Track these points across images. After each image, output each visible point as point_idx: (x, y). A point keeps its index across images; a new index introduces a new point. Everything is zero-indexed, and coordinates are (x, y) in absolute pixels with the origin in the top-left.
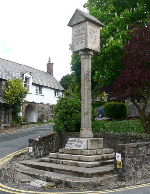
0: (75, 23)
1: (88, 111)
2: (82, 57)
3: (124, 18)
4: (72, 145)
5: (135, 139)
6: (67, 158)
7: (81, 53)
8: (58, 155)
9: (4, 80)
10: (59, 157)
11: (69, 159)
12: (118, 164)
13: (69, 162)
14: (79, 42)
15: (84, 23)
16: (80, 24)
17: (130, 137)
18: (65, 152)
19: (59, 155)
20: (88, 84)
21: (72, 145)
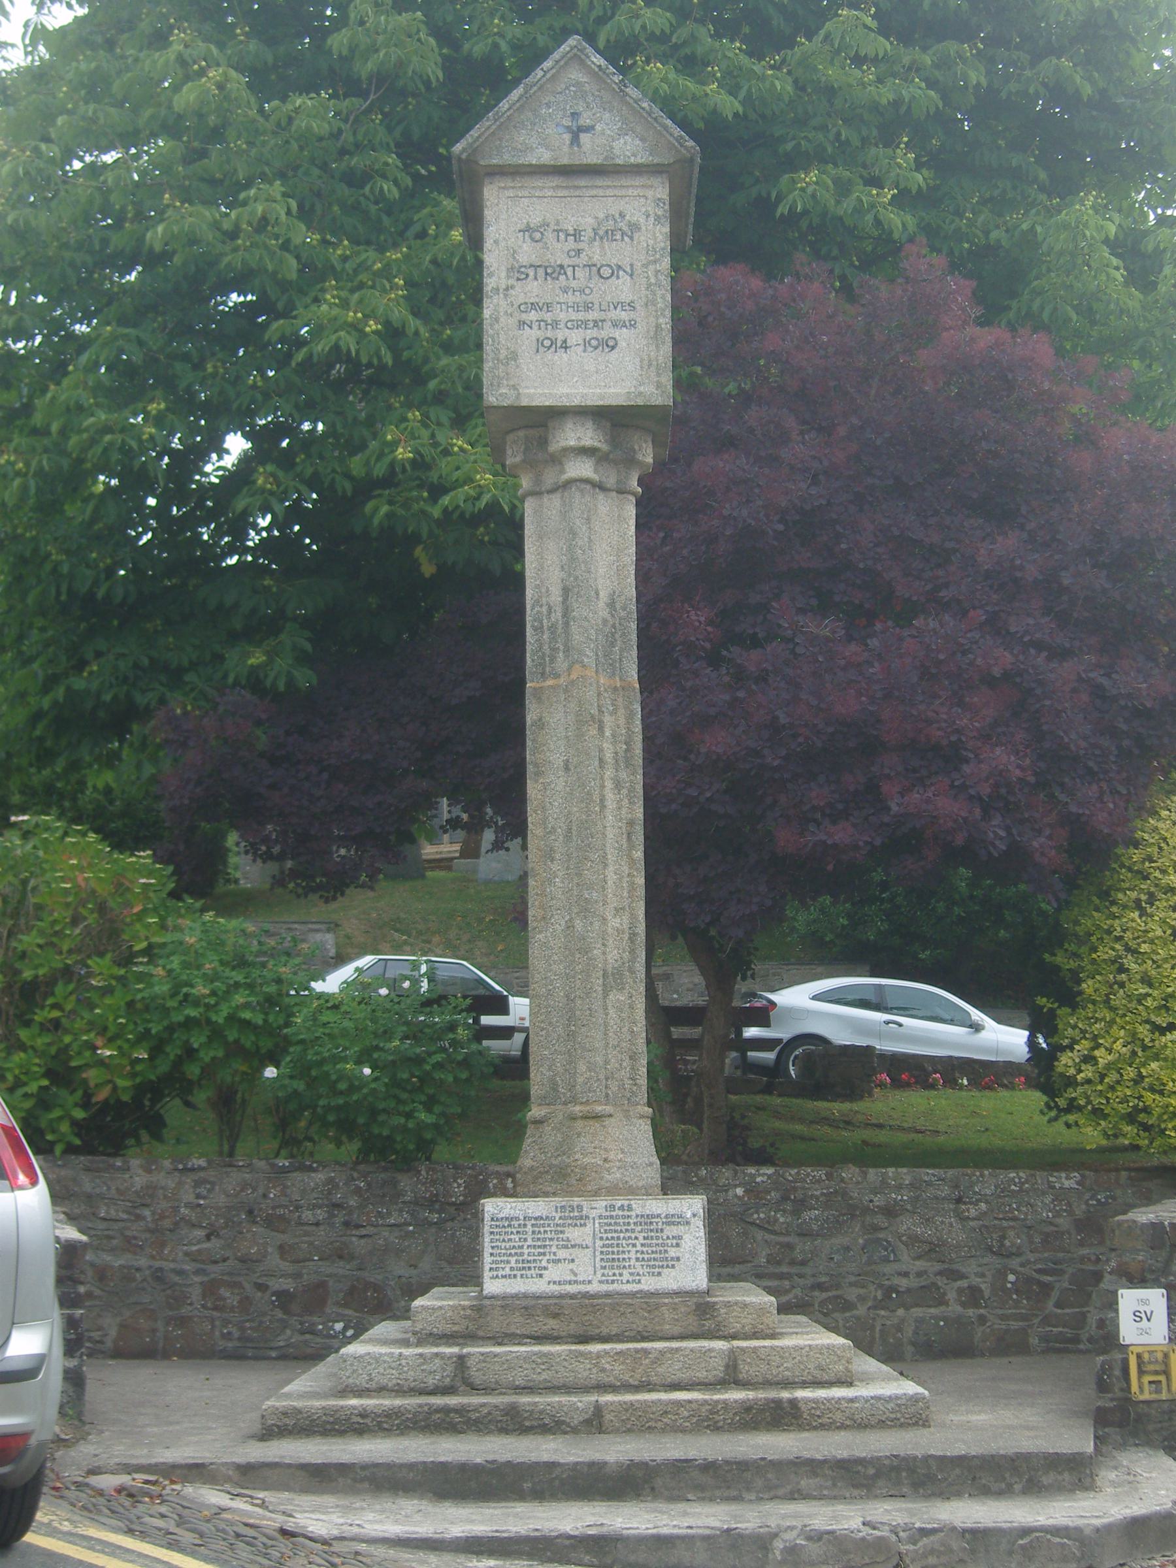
0: (543, 156)
1: (626, 955)
2: (582, 468)
3: (296, 512)
4: (562, 1254)
5: (785, 1198)
6: (564, 1375)
7: (574, 435)
8: (461, 1358)
9: (316, 165)
10: (477, 1377)
11: (606, 1379)
12: (1141, 1372)
13: (679, 1404)
14: (575, 337)
15: (639, 181)
16: (582, 182)
17: (739, 1191)
18: (496, 1323)
19: (470, 1362)
20: (622, 721)
21: (562, 1254)
